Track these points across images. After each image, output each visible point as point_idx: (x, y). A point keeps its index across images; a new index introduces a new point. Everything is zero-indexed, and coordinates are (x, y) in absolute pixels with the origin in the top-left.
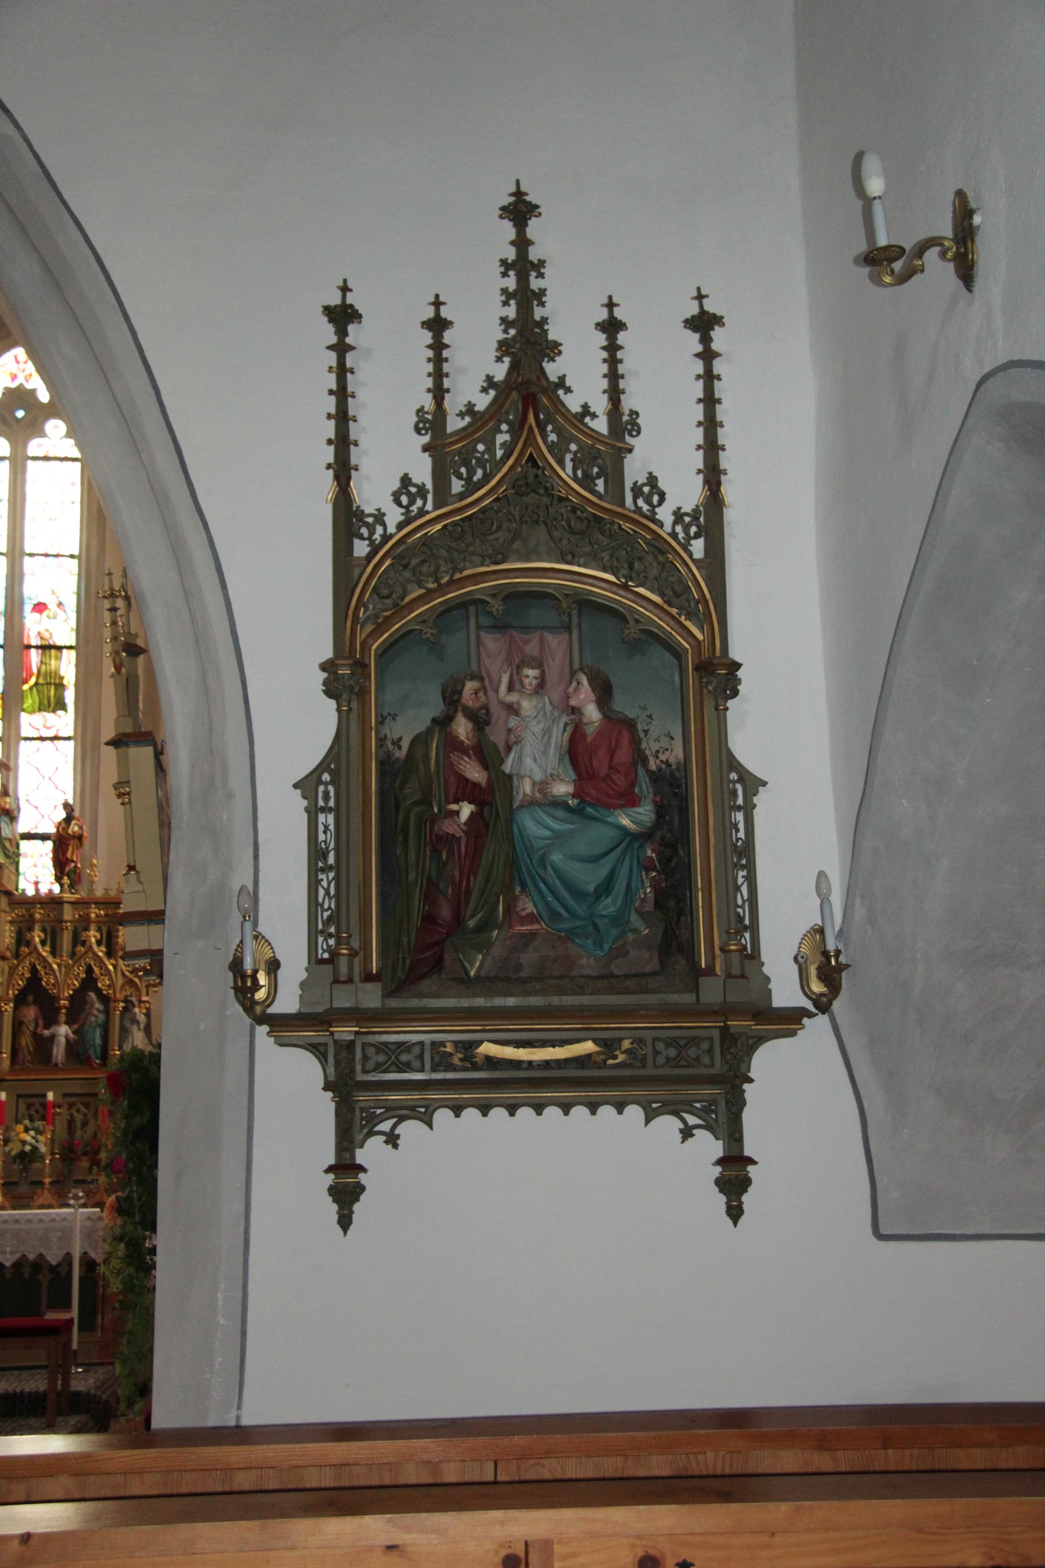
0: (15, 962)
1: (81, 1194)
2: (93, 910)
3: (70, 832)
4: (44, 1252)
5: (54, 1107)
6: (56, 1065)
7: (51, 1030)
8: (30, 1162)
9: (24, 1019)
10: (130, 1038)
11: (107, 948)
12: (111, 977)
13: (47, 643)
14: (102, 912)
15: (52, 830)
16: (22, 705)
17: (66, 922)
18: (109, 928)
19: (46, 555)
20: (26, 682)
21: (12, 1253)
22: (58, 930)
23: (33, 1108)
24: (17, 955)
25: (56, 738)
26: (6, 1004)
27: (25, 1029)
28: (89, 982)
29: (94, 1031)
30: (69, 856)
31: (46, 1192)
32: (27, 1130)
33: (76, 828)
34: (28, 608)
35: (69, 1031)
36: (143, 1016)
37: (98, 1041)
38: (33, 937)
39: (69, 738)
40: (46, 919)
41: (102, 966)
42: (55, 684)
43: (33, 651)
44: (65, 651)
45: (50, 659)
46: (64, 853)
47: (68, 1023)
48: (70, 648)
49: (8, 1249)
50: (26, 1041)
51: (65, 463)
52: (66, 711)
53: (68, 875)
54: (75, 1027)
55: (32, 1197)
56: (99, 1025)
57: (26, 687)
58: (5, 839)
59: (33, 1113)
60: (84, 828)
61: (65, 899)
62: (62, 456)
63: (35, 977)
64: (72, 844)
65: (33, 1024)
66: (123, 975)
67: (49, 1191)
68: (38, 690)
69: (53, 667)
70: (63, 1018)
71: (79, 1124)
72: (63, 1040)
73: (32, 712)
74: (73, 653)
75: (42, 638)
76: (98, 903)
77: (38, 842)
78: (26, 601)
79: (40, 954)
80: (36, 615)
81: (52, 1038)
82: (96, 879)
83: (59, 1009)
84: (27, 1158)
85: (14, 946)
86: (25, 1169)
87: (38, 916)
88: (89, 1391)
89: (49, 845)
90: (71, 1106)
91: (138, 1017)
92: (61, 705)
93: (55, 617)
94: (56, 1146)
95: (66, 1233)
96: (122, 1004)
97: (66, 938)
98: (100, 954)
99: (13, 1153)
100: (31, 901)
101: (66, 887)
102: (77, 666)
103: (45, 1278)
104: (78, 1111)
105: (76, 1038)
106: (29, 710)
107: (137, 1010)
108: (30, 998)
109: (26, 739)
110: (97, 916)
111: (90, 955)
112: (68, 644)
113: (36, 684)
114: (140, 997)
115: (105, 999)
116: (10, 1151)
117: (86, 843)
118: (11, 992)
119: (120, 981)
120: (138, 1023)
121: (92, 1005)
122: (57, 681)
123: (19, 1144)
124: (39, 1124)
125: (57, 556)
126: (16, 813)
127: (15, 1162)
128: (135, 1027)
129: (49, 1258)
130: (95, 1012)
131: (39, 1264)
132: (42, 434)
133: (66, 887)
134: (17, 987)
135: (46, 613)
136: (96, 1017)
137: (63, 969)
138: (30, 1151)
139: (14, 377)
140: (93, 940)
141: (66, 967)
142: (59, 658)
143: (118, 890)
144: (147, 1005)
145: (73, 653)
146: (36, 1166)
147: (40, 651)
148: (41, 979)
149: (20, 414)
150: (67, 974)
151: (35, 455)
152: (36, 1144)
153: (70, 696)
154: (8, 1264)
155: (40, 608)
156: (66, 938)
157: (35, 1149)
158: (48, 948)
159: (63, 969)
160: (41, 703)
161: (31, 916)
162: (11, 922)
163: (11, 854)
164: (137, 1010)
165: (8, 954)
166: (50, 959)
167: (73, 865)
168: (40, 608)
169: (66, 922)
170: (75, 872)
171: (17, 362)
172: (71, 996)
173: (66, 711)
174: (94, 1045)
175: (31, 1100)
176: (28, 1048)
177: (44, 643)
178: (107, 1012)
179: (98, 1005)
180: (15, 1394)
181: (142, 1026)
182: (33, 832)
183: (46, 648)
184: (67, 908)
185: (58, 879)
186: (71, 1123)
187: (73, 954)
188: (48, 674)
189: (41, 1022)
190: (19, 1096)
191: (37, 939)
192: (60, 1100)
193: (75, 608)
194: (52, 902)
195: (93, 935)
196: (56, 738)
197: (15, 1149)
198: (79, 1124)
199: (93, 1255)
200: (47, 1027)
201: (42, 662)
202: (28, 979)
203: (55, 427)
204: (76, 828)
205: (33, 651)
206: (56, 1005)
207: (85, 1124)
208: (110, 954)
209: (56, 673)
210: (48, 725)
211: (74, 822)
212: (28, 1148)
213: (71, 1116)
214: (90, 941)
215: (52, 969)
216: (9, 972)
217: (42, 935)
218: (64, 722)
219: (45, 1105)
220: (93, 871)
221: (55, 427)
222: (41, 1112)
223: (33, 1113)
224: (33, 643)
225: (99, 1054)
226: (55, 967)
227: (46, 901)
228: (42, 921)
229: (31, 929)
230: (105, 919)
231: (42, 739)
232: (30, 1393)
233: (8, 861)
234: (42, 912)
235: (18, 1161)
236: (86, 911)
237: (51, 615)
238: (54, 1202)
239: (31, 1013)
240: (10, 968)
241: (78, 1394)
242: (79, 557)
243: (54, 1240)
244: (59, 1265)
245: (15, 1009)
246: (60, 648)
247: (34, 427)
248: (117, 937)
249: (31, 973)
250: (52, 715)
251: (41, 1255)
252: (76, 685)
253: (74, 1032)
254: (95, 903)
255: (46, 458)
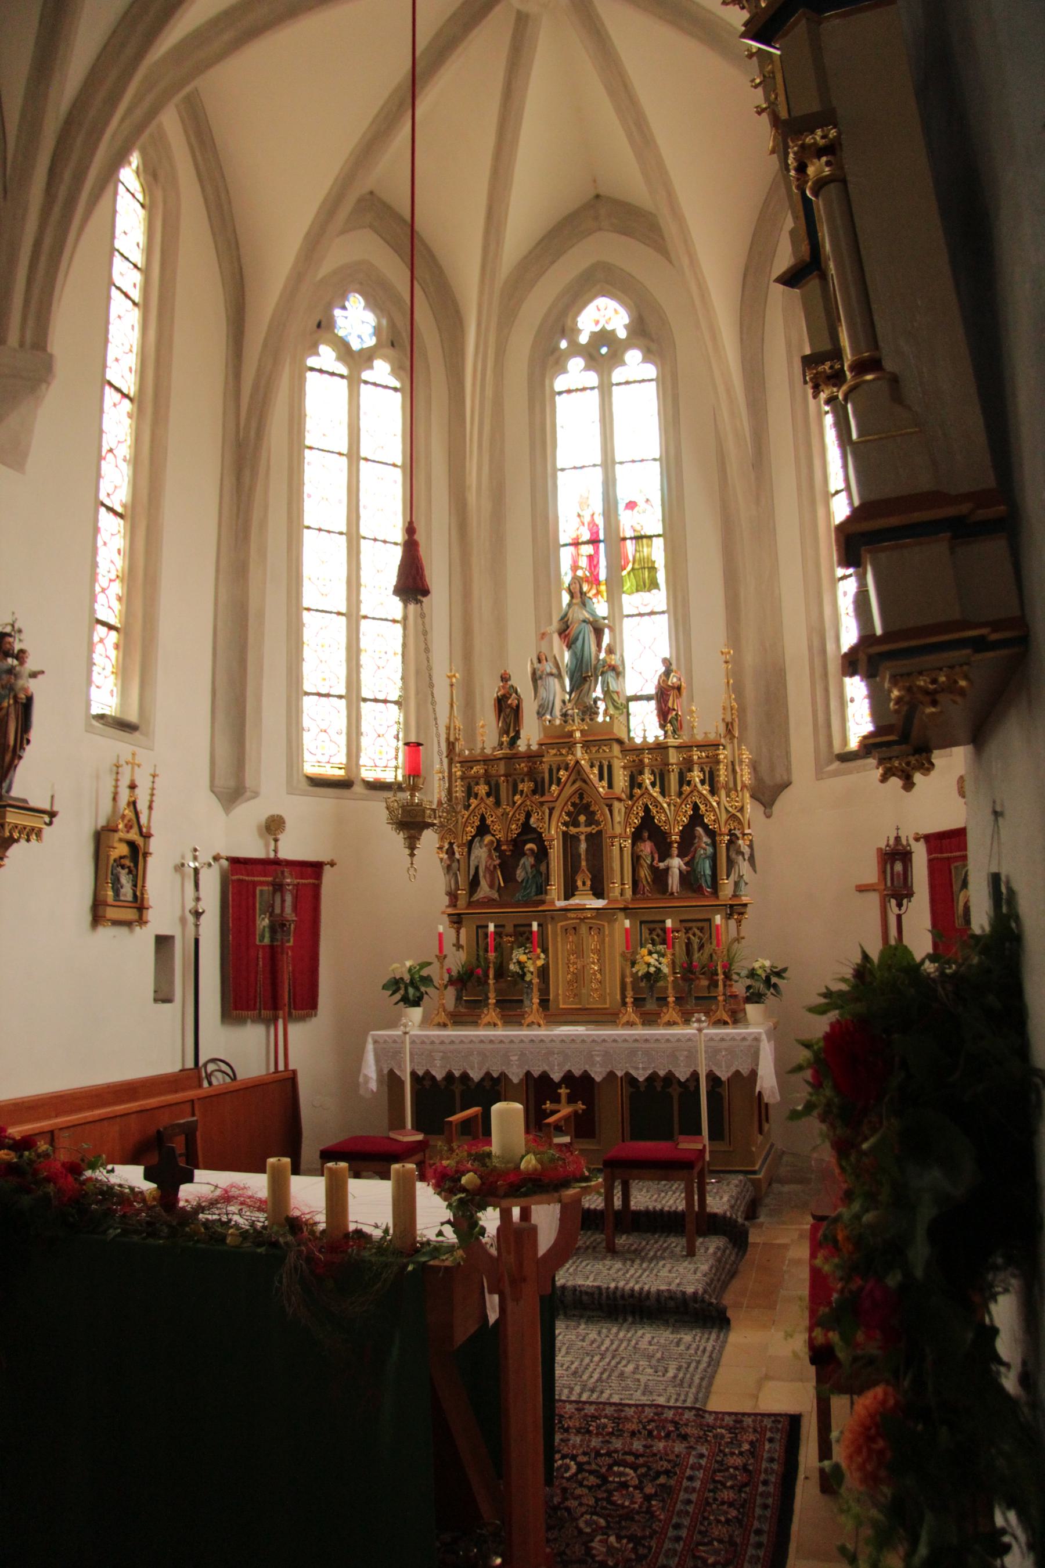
0: (630, 802)
1: (703, 1018)
2: (694, 753)
3: (670, 683)
4: (673, 1070)
5: (673, 932)
6: (672, 894)
7: (666, 863)
8: (656, 981)
9: (641, 853)
10: (737, 867)
11: (710, 786)
12: (666, 813)
13: (639, 534)
14: (703, 754)
15: (651, 690)
16: (623, 588)
17: (672, 765)
18: (711, 768)
19: (633, 461)
20: (624, 568)
21: (644, 1069)
22: (666, 773)
23: (655, 933)
24: (631, 797)
25: (652, 613)
26: (625, 841)
27: (642, 861)
28: (696, 818)
29: (704, 863)
30: (670, 705)
31: (671, 1010)
32: (650, 953)
33: (675, 680)
34: (621, 506)
35: (682, 863)
36: (746, 847)
37: (708, 872)
38: (643, 780)
39: (663, 612)
40: (655, 763)
41: (707, 802)
42: (648, 568)
43: (628, 542)
44: (654, 539)
45: (643, 547)
46: (666, 702)
47: (681, 855)
48: (659, 536)
49: (641, 1066)
50: (644, 873)
51: (643, 384)
52: (659, 590)
53: (670, 722)
54: (687, 859)
55: (660, 1014)
56: (707, 857)
57: (624, 573)
58: (613, 692)
59: (655, 937)
60: (682, 679)
61: (669, 744)
62: (640, 379)
63: (648, 818)
64: (672, 694)
65: (649, 858)
66: (726, 808)
67: (674, 1009)
68: (634, 575)
69: (645, 554)
70: (675, 851)
71: (696, 947)
72: (677, 871)
73: (632, 593)
74: (661, 539)
75: (634, 531)
76: (700, 747)
77: (644, 702)
78: (620, 501)
79: (651, 795)
80: (629, 512)
81: (667, 869)
82: (696, 724)
83: (671, 843)
84: (652, 978)
85: (628, 789)
86: (651, 988)
87: (646, 761)
88: (725, 1213)
89: (653, 704)
90: (687, 930)
91: (742, 849)
92: (654, 585)
93: (644, 512)
94: (677, 967)
95: (692, 1055)
96: (727, 838)
97: (673, 779)
98: (704, 792)
99: (640, 974)
100: (639, 747)
101: (670, 733)
102: (665, 550)
103: (675, 1092)
104: (694, 935)
105: (689, 869)
106: (629, 591)
107: (740, 842)
108: (646, 835)
109: (628, 616)
110: (699, 758)
111: (696, 793)
112: (656, 534)
113: (633, 569)
114: (743, 831)
115: (712, 834)
116: (637, 972)
117: (684, 692)
118: (628, 830)
119: (724, 817)
120: (743, 854)
121: (700, 838)
122: (650, 565)
123: (645, 966)
124: (661, 948)
125: (642, 461)
126: (621, 669)
127: (642, 981)
128: (741, 857)
129: (677, 1075)
130: (704, 845)
131: (670, 1078)
132: (622, 363)
133: (670, 733)
134: (633, 825)
135: (636, 509)
136: (705, 849)
137: (672, 808)
138: (655, 972)
139: (597, 323)
140: (697, 780)
141: (675, 806)
142: (650, 546)
143: (716, 733)
144: (750, 837)
145: (661, 539)
146: (661, 984)
147: (634, 541)
148: (654, 817)
149: (604, 350)
150: (676, 814)
151: (618, 382)
152: (659, 966)
153: (661, 577)
154: (641, 1079)
155: (631, 505)
156: (673, 779)
157: (658, 970)
158: (657, 789)
159: (672, 808)
160: (637, 586)
161: (641, 761)
162: (624, 768)
163: (619, 705)
164: (740, 842)
165: (624, 796)
166: (660, 799)
167: (674, 713)
168: (631, 505)
169: (672, 765)
170: (677, 720)
171: (599, 310)
172: (681, 831)
173: (659, 590)
174: (705, 875)
175: (652, 926)
176: (647, 880)
177: (638, 534)
178: (714, 844)
179: (706, 839)
180: (655, 1211)
181: (746, 857)
182: (638, 694)
183: (638, 538)
184: (671, 751)
185: (662, 726)
186: (689, 945)
187: (680, 794)
188: (642, 560)
189: (656, 856)
190: (641, 923)
191: (648, 781)
192: (678, 925)
193: (660, 503)
194: (660, 748)
195: (696, 776)
196: (652, 613)
197: (641, 969)
198: (696, 947)
199: (718, 1074)
200: (661, 860)
201: (636, 550)
202: (642, 818)
203: (633, 356)
204: (675, 680)
205: (628, 542)
206: (669, 840)
207: (701, 947)
208: (713, 792)
209: (648, 559)
210: (645, 603)
211: (672, 674)
212: (652, 970)
213: (689, 939)
214: (694, 780)
215: (662, 808)
216: (625, 813)
217: (652, 778)
218: (658, 599)
219: (664, 930)
220: (693, 717)
221: (633, 356)
222: (660, 937)
223: (655, 937)
224: (628, 536)
225: (709, 883)
226: (665, 805)
227: (652, 746)
228: (651, 766)
229: (641, 773)
230: (706, 760)
231: (641, 615)
232: (669, 1212)
233: (617, 712)
234: (650, 756)
235: (644, 980)
236: (689, 753)
237: (641, 511)
238: (678, 1020)
239: (647, 848)
240: (626, 808)
241: (715, 1215)
242: (660, 460)
243: (682, 1059)
244: (687, 1080)
245: (633, 844)
246: (650, 537)
247: (616, 358)
248: (718, 776)
249: (480, 821)
250: (648, 593)
251: (586, 1071)
252: (666, 566)
253: (685, 864)
254: (696, 746)
255: (627, 383)
